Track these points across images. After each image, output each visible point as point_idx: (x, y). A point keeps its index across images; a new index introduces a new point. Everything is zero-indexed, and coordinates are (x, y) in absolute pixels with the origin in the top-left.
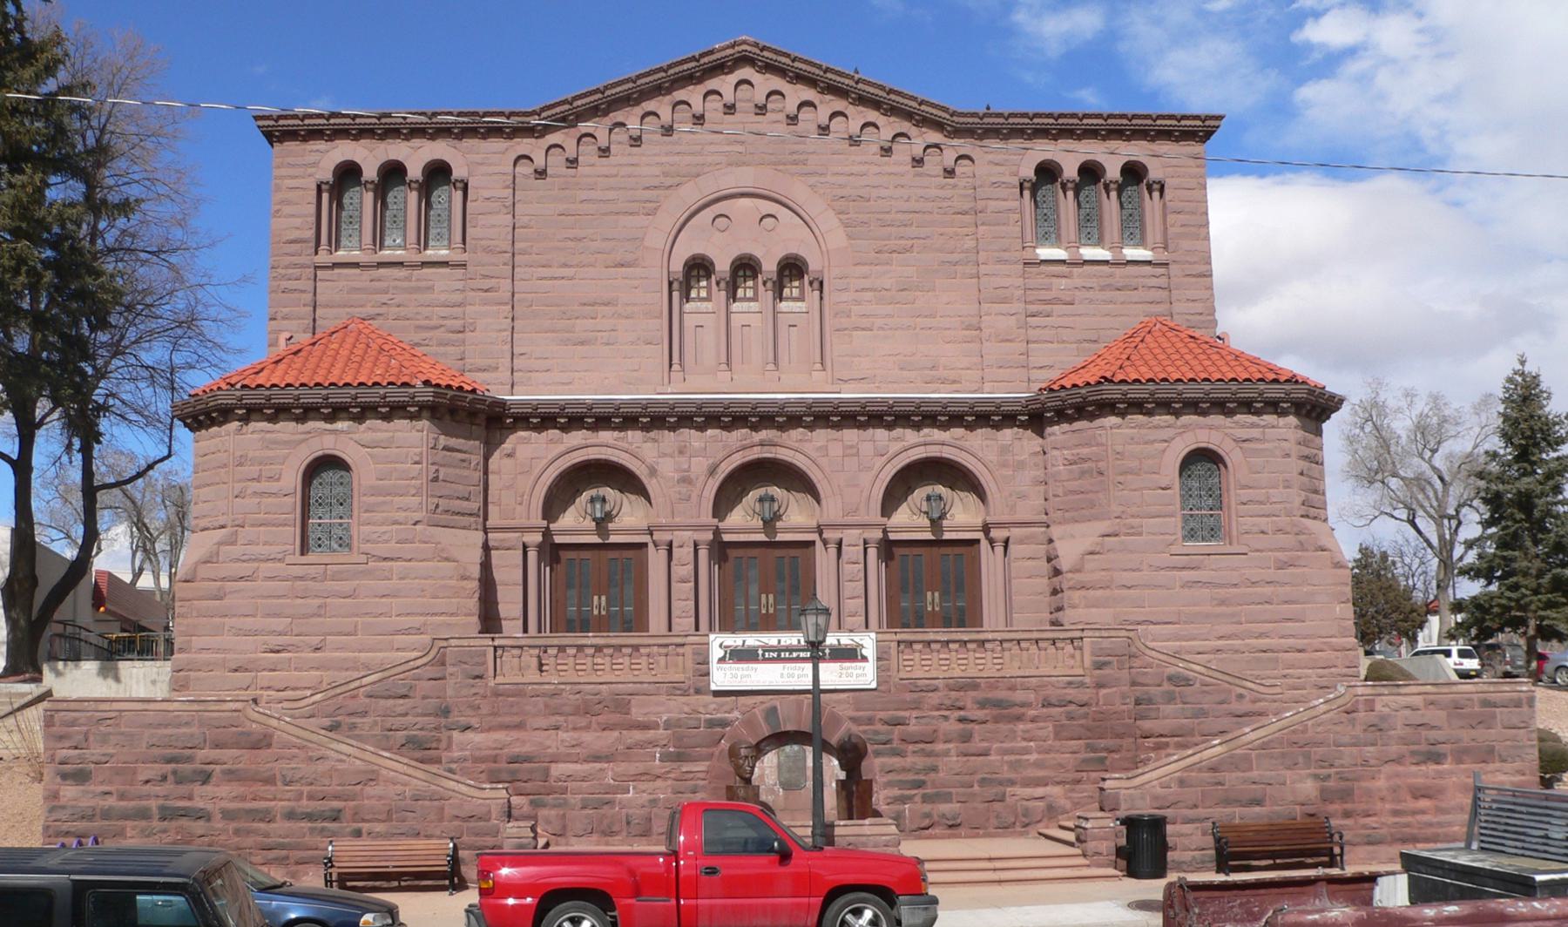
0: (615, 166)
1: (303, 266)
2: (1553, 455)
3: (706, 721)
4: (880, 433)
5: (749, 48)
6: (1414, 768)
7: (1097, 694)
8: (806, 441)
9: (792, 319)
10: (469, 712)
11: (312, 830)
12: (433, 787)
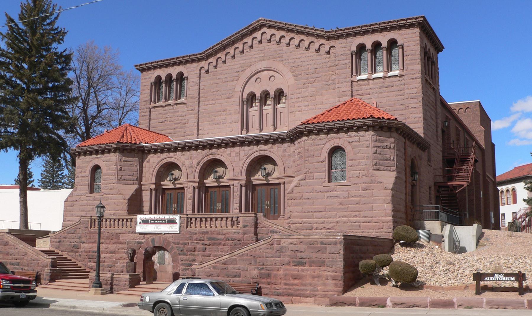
1: (146, 108)
6: (294, 267)
7: (244, 236)
8: (224, 152)
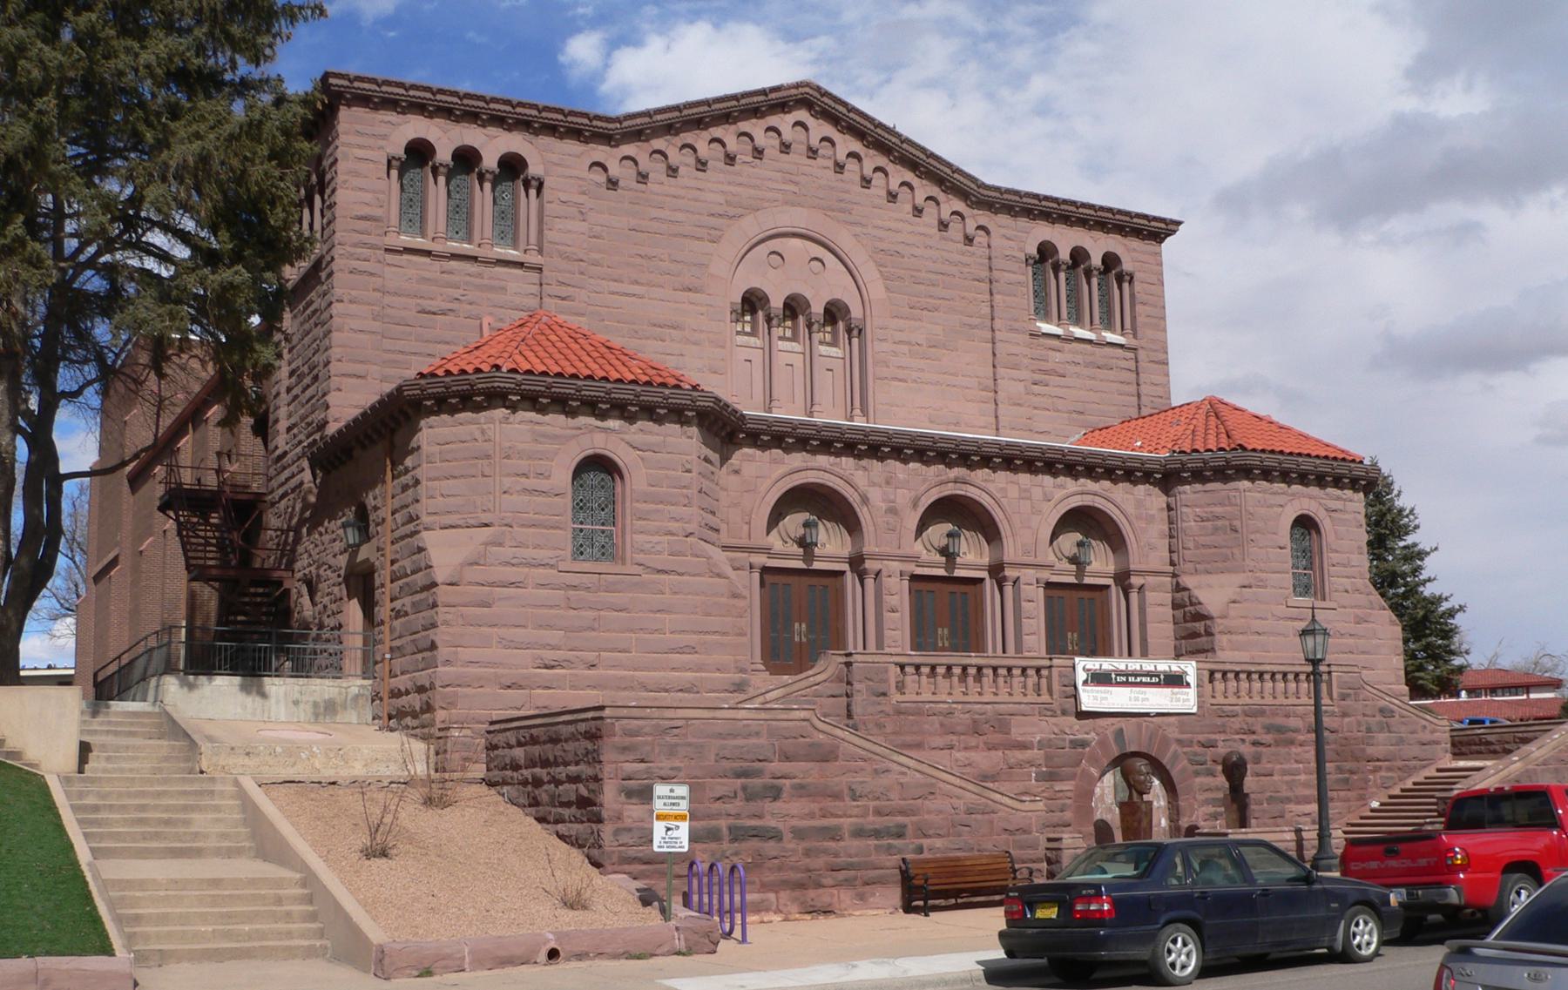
0: (683, 188)
2: (1402, 544)
3: (1071, 742)
4: (1047, 480)
5: (811, 92)
9: (828, 363)
10: (875, 731)
11: (877, 848)
12: (984, 800)
